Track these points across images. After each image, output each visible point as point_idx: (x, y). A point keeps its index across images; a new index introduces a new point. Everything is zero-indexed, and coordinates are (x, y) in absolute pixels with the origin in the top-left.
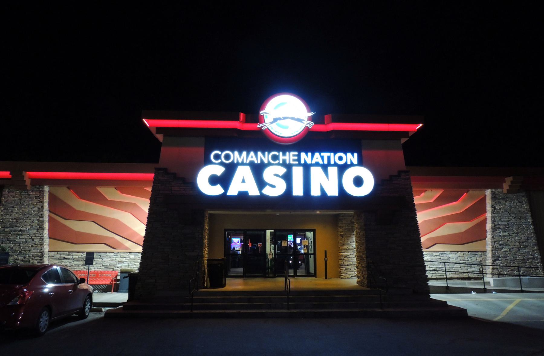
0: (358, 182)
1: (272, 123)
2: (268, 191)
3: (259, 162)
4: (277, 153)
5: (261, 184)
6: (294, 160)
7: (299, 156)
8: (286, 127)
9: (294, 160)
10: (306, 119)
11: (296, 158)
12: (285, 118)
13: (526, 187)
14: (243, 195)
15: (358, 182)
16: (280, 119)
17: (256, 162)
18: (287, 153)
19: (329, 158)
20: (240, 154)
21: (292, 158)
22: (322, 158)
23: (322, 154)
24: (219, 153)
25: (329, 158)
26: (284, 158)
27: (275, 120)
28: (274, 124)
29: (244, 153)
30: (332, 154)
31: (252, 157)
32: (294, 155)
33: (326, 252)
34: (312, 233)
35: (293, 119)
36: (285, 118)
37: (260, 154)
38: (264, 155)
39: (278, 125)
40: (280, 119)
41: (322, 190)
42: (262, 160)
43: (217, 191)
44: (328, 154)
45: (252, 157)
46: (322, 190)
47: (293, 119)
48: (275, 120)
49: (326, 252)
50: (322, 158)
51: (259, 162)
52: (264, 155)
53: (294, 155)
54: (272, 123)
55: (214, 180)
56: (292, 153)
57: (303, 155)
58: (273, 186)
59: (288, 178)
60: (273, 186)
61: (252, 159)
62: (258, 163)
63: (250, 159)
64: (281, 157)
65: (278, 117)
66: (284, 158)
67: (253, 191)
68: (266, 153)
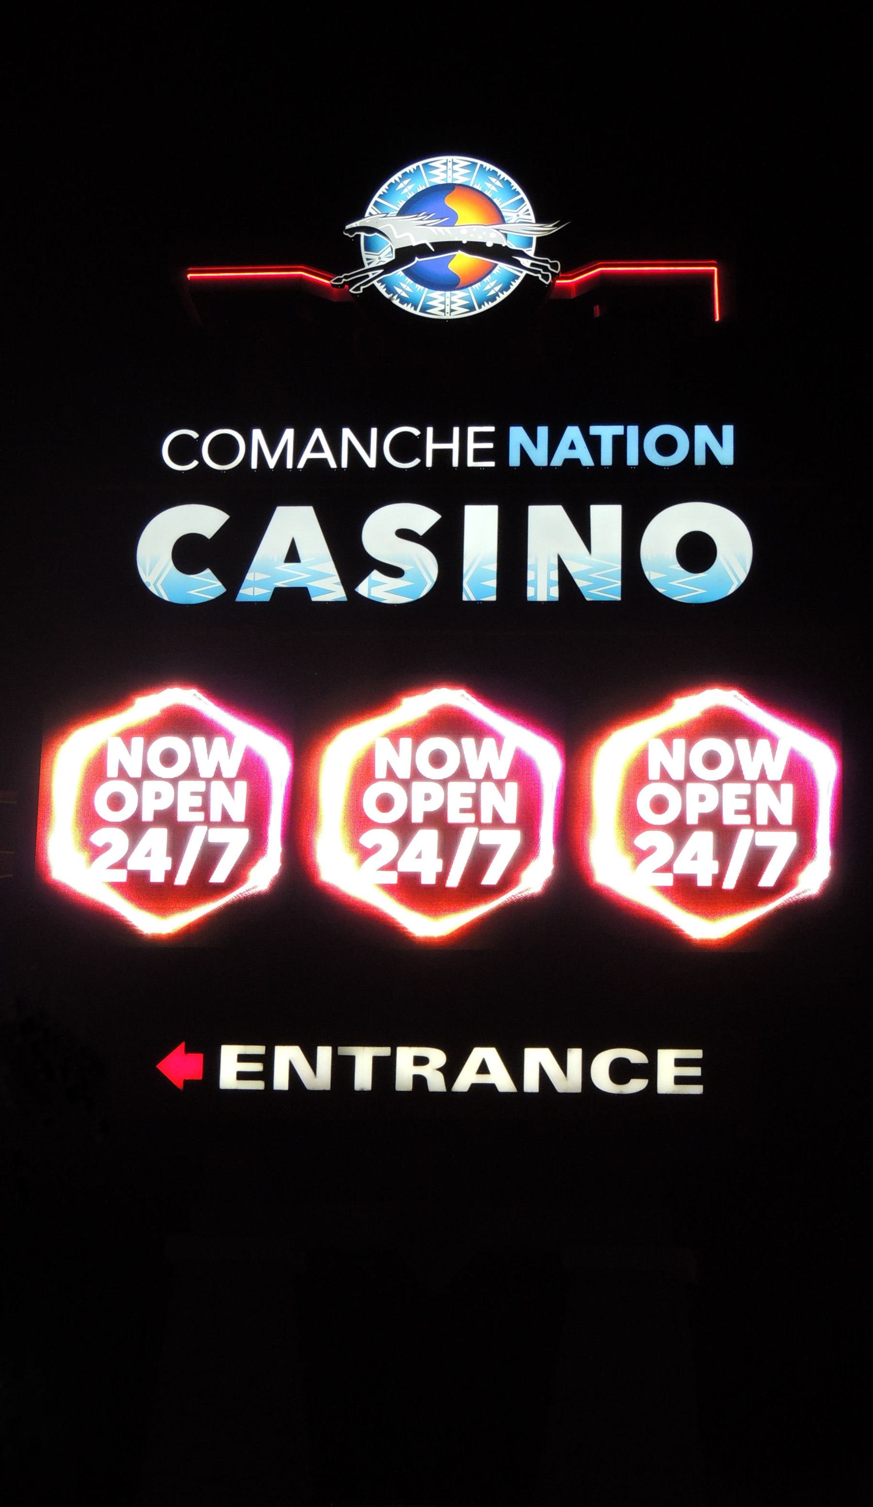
0: (697, 552)
1: (389, 268)
2: (376, 588)
5: (353, 562)
7: (501, 440)
8: (451, 284)
9: (480, 455)
13: (458, 887)
14: (292, 599)
15: (697, 552)
19: (620, 443)
22: (594, 444)
23: (594, 430)
25: (620, 443)
28: (399, 272)
30: (633, 431)
31: (318, 448)
32: (479, 437)
39: (415, 276)
41: (565, 578)
43: (205, 586)
44: (619, 430)
45: (318, 448)
46: (565, 578)
48: (404, 255)
50: (594, 444)
53: (479, 437)
55: (189, 553)
57: (517, 435)
58: (405, 534)
59: (446, 542)
60: (405, 534)
67: (328, 588)
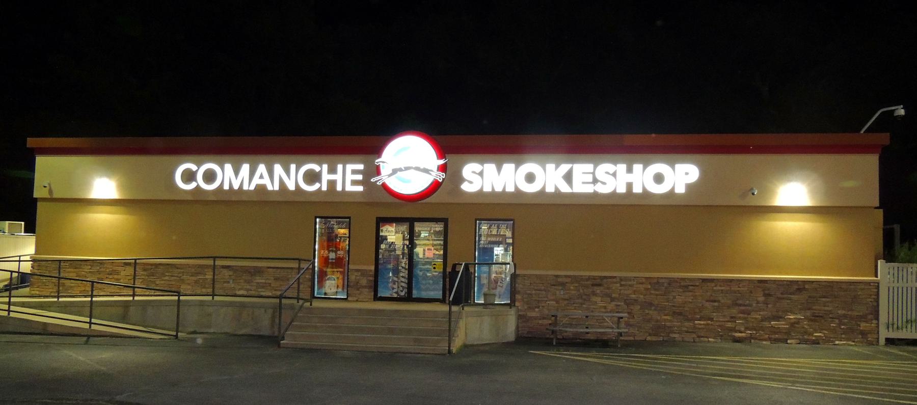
1: (390, 176)
3: (277, 188)
4: (315, 167)
6: (354, 183)
9: (354, 183)
10: (435, 169)
11: (360, 177)
12: (407, 169)
16: (400, 170)
17: (270, 188)
18: (340, 167)
20: (237, 172)
21: (350, 177)
24: (193, 167)
26: (332, 177)
27: (395, 171)
29: (245, 168)
31: (261, 177)
32: (354, 172)
33: (583, 183)
34: (441, 297)
35: (417, 169)
36: (407, 169)
37: (278, 169)
38: (287, 172)
40: (400, 170)
42: (282, 182)
45: (261, 177)
47: (417, 169)
48: (395, 171)
49: (583, 183)
51: (277, 188)
52: (287, 172)
53: (354, 172)
54: (390, 176)
56: (350, 167)
61: (261, 182)
62: (273, 191)
63: (256, 181)
64: (326, 177)
65: (398, 167)
66: (332, 177)
68: (293, 167)
